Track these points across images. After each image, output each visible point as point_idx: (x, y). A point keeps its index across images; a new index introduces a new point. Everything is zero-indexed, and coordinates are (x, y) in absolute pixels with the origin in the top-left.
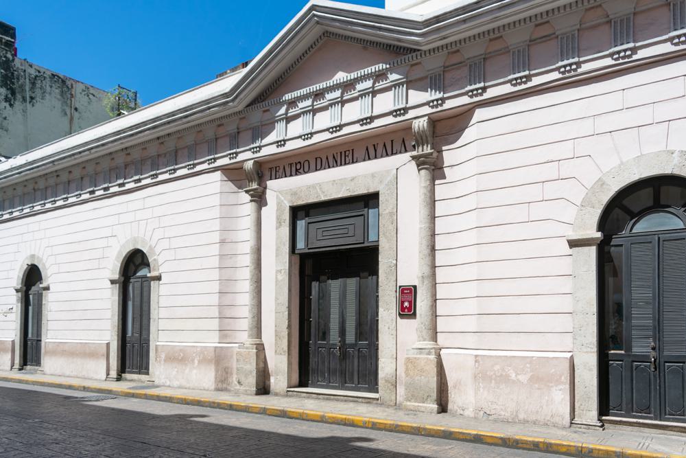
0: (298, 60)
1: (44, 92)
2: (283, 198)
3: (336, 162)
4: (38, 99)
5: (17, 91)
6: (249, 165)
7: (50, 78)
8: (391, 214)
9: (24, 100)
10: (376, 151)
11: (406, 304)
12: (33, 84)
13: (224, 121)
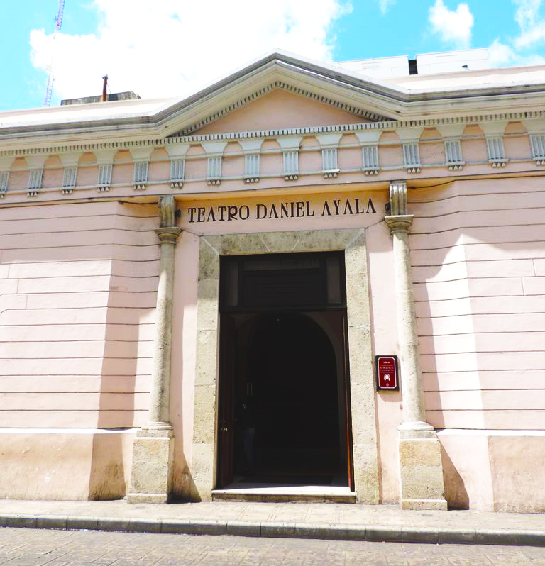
0: (253, 95)
2: (210, 245)
3: (286, 213)
8: (361, 275)
10: (337, 208)
11: (387, 377)
13: (130, 147)
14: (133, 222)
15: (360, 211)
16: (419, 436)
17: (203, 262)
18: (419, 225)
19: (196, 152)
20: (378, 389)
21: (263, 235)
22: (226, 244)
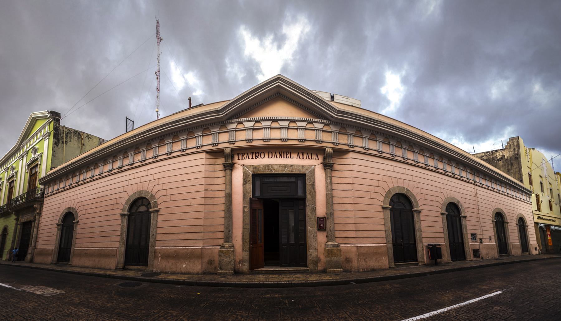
1: (71, 139)
2: (247, 170)
4: (68, 142)
5: (60, 139)
6: (228, 150)
7: (74, 132)
9: (63, 143)
11: (322, 225)
12: (67, 135)
14: (212, 161)
15: (313, 158)
16: (334, 247)
17: (244, 177)
18: (336, 167)
19: (240, 126)
20: (318, 230)
21: (271, 166)
22: (255, 170)
